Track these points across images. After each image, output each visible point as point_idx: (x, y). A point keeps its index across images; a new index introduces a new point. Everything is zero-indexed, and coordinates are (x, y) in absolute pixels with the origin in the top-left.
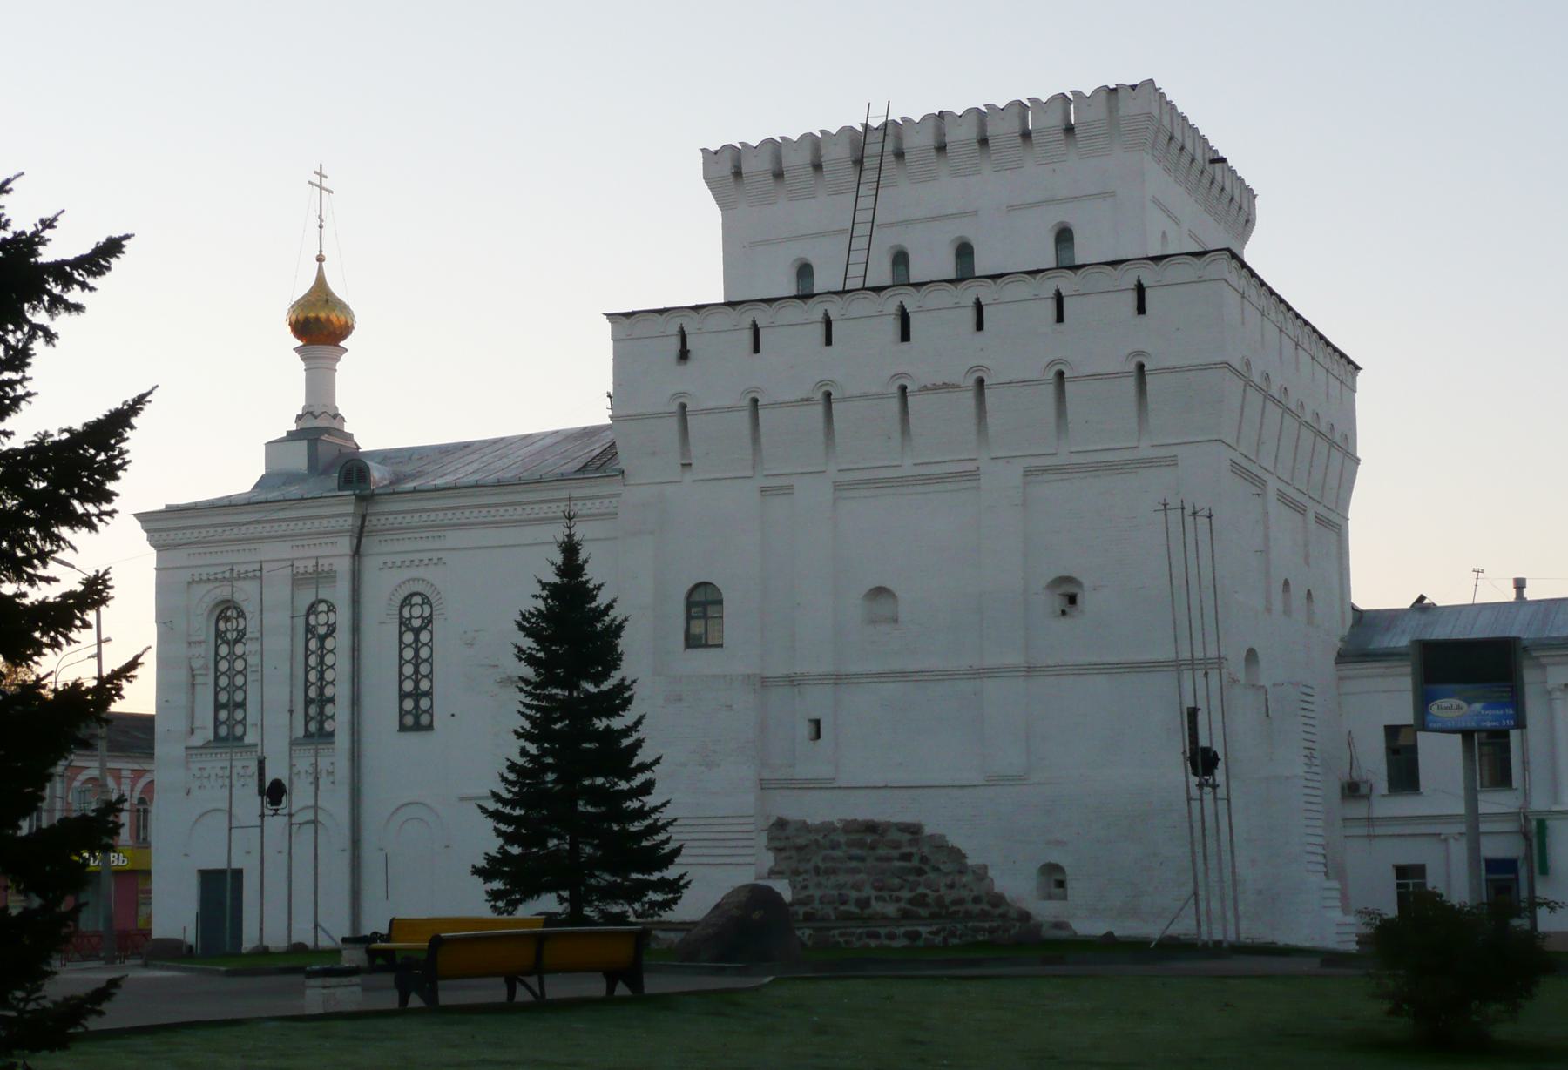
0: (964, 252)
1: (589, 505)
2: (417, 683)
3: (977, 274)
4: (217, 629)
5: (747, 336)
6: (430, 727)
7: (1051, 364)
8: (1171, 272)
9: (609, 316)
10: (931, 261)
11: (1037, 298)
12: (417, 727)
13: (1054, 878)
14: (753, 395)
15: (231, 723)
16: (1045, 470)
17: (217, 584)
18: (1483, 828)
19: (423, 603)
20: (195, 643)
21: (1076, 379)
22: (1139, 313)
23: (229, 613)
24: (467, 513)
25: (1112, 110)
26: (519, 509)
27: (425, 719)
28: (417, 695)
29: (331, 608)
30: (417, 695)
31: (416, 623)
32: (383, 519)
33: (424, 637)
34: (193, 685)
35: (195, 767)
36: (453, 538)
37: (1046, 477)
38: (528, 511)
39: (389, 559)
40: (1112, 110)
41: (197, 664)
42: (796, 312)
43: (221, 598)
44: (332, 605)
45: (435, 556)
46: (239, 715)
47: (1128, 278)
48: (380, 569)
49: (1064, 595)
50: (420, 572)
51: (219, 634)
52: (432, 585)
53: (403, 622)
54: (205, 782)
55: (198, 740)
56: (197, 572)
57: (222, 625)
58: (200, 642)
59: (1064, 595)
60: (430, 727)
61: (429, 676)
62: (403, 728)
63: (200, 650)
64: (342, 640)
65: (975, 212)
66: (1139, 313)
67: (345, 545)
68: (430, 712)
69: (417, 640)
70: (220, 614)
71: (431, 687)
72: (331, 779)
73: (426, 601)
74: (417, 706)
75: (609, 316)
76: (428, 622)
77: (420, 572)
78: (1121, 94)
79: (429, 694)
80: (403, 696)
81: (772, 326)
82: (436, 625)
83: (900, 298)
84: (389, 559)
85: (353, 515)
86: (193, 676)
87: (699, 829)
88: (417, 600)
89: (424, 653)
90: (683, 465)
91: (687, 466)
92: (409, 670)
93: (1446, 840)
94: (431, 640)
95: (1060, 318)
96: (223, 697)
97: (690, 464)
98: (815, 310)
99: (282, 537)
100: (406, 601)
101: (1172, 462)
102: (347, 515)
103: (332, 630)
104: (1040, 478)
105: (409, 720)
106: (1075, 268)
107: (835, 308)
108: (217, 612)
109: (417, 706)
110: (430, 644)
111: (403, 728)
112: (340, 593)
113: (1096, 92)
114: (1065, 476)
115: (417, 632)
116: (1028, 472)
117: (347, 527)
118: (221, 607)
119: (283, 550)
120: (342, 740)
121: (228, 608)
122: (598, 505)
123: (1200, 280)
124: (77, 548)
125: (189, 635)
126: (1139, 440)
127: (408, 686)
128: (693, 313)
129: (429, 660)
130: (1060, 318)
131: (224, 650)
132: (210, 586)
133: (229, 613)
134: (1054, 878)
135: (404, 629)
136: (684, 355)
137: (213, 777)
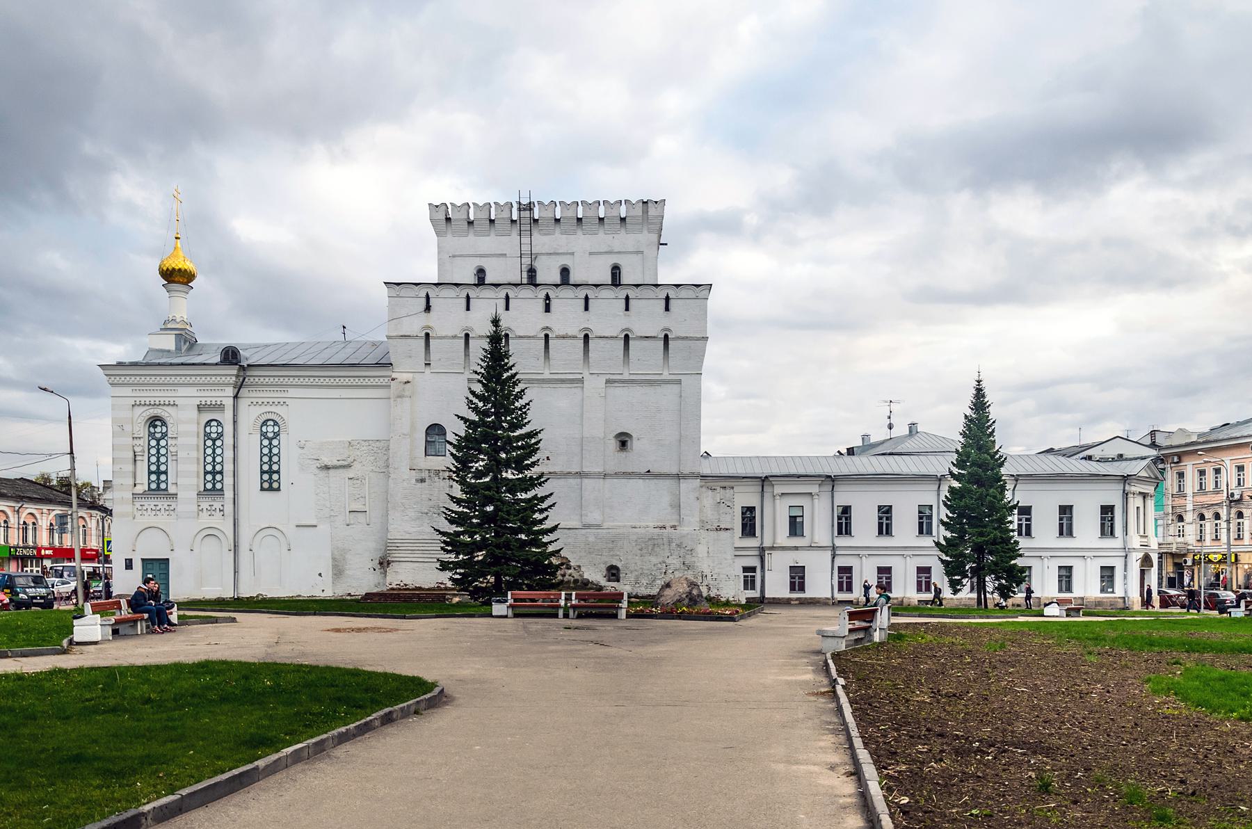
0: (565, 272)
1: (332, 381)
2: (158, 467)
3: (486, 283)
4: (149, 431)
5: (464, 302)
6: (278, 489)
7: (623, 330)
8: (683, 293)
9: (385, 283)
10: (548, 273)
11: (617, 298)
12: (271, 489)
13: (613, 573)
14: (666, 332)
15: (270, 481)
16: (615, 381)
17: (150, 407)
18: (837, 552)
19: (274, 425)
20: (136, 438)
21: (674, 339)
22: (546, 312)
23: (156, 423)
24: (302, 379)
25: (645, 212)
26: (203, 378)
27: (275, 485)
28: (271, 472)
29: (219, 424)
30: (271, 472)
31: (214, 436)
32: (252, 379)
33: (218, 443)
34: (135, 461)
35: (138, 505)
36: (293, 392)
37: (616, 385)
38: (347, 381)
39: (255, 401)
40: (645, 212)
41: (137, 449)
42: (527, 292)
43: (153, 415)
44: (220, 422)
45: (282, 401)
46: (275, 477)
47: (582, 293)
48: (249, 405)
49: (620, 441)
50: (273, 409)
51: (150, 434)
52: (282, 418)
53: (264, 435)
54: (158, 513)
55: (140, 489)
56: (138, 400)
57: (152, 430)
58: (140, 438)
59: (620, 441)
60: (278, 489)
61: (278, 463)
62: (262, 489)
63: (141, 442)
64: (228, 439)
65: (573, 254)
66: (666, 311)
67: (230, 391)
68: (278, 481)
69: (158, 444)
70: (151, 423)
71: (279, 468)
72: (222, 513)
73: (276, 423)
74: (271, 478)
75: (385, 283)
76: (277, 435)
77: (273, 409)
78: (650, 204)
79: (278, 472)
80: (263, 472)
81: (516, 298)
82: (283, 436)
83: (548, 291)
84: (255, 401)
85: (237, 376)
86: (135, 456)
87: (433, 545)
88: (214, 423)
89: (275, 451)
90: (426, 364)
91: (428, 364)
92: (266, 459)
93: (861, 558)
94: (222, 444)
95: (627, 309)
96: (209, 468)
97: (430, 364)
98: (622, 293)
99: (128, 385)
100: (265, 423)
101: (679, 382)
102: (233, 375)
103: (220, 435)
104: (612, 385)
105: (266, 485)
106: (536, 285)
107: (632, 293)
108: (149, 423)
109: (271, 478)
110: (278, 446)
111: (262, 489)
112: (226, 418)
113: (638, 202)
114: (626, 385)
115: (270, 440)
116: (608, 381)
117: (231, 382)
118: (151, 420)
119: (192, 391)
120: (229, 494)
121: (156, 420)
122: (342, 381)
123: (697, 298)
124: (431, 325)
125: (133, 434)
126: (663, 370)
127: (266, 467)
128: (434, 287)
129: (278, 455)
130: (627, 309)
131: (266, 442)
132: (147, 408)
133: (156, 423)
134: (613, 573)
135: (263, 438)
136: (428, 308)
137: (149, 510)
